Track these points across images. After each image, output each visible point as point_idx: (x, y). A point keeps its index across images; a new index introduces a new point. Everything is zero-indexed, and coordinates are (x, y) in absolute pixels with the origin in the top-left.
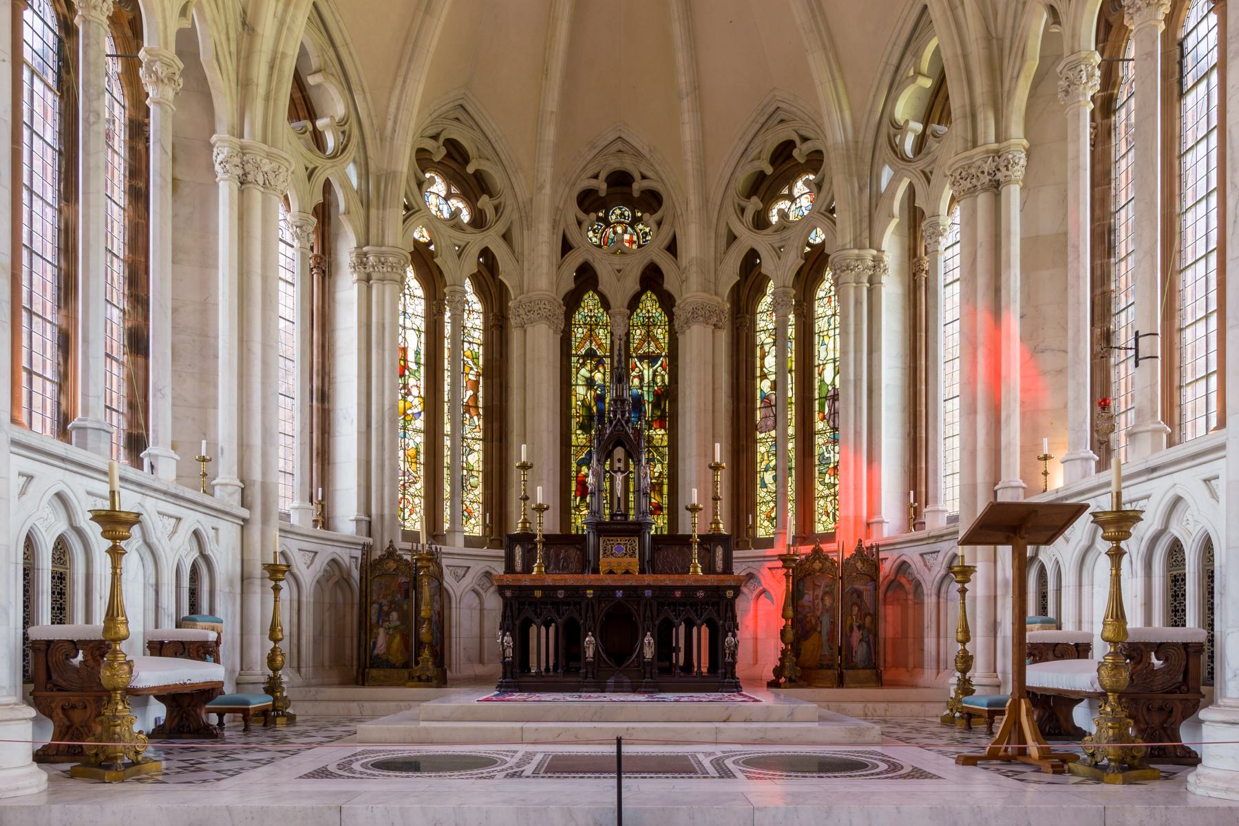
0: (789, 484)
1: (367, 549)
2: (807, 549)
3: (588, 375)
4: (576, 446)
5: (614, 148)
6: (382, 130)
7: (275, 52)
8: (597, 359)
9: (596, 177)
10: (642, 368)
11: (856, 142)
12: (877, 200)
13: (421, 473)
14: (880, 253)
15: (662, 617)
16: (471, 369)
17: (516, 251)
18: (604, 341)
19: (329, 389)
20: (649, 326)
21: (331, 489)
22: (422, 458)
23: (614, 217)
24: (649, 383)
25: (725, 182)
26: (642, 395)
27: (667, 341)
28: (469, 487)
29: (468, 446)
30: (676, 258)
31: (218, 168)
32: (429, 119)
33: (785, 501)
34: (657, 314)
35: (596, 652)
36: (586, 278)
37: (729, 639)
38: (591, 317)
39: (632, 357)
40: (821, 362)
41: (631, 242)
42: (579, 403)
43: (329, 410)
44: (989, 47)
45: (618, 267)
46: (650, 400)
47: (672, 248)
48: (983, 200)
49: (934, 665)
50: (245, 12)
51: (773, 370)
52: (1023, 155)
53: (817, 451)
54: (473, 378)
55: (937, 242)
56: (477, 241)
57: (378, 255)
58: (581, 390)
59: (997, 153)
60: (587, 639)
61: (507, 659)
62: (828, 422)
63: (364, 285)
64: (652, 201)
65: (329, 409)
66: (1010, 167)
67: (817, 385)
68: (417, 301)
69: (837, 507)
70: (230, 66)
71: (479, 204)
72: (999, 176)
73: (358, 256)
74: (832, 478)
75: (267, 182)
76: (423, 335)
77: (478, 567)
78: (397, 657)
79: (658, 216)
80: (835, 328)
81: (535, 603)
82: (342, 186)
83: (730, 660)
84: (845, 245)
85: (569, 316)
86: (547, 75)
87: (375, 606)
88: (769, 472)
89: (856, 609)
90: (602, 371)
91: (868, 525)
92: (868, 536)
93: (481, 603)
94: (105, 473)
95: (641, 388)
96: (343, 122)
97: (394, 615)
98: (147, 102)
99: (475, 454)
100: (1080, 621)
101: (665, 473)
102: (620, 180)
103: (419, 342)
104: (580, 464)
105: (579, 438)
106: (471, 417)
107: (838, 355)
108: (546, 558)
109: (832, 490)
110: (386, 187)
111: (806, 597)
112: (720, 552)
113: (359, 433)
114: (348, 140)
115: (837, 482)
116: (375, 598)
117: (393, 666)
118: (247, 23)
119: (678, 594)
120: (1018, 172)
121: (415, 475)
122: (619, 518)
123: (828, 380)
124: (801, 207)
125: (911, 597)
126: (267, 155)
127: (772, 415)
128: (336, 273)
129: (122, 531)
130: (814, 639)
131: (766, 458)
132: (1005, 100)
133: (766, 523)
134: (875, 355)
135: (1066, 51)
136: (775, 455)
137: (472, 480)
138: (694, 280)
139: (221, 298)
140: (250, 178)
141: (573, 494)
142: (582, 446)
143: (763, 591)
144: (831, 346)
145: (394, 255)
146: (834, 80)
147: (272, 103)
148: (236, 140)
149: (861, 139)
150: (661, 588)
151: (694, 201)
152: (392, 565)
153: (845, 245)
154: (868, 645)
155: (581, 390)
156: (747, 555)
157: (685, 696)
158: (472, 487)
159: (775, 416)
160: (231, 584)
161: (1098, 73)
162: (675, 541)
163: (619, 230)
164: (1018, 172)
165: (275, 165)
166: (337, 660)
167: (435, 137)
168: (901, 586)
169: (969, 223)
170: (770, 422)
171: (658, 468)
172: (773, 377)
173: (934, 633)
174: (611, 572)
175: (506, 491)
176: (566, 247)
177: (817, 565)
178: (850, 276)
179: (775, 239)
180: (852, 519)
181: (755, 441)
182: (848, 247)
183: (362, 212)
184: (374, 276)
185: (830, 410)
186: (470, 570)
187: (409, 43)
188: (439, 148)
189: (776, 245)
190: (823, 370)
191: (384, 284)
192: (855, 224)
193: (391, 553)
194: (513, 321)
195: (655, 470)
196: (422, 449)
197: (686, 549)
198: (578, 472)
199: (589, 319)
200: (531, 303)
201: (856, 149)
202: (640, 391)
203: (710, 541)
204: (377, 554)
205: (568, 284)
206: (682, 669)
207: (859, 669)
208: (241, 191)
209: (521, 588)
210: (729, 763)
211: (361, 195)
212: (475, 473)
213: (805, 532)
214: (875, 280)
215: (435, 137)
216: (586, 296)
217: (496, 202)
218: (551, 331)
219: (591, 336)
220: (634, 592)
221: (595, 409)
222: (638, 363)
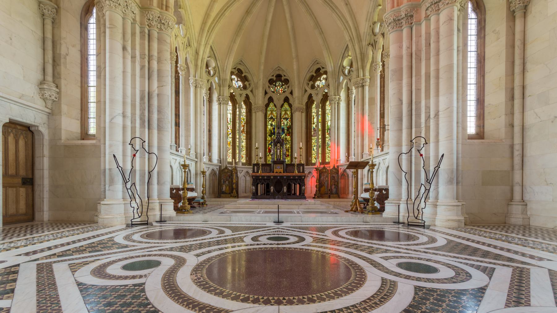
1: (220, 167)
2: (322, 166)
5: (278, 69)
6: (223, 69)
7: (202, 58)
9: (273, 76)
11: (334, 70)
13: (231, 148)
15: (288, 183)
22: (231, 144)
30: (292, 95)
31: (190, 84)
35: (273, 190)
36: (271, 100)
37: (303, 187)
41: (281, 90)
44: (361, 55)
47: (291, 93)
48: (360, 89)
49: (351, 193)
50: (196, 50)
53: (326, 142)
54: (243, 124)
55: (352, 96)
56: (244, 93)
57: (223, 98)
58: (269, 127)
59: (363, 79)
64: (287, 81)
67: (326, 126)
68: (230, 106)
70: (193, 62)
71: (245, 83)
72: (363, 84)
73: (218, 98)
77: (245, 170)
78: (228, 192)
79: (288, 85)
81: (259, 179)
82: (214, 83)
85: (266, 109)
89: (333, 180)
91: (337, 160)
92: (337, 163)
93: (246, 179)
94: (183, 157)
95: (284, 126)
96: (214, 68)
97: (227, 182)
100: (377, 184)
102: (279, 77)
103: (231, 116)
104: (269, 145)
105: (269, 138)
108: (262, 169)
111: (322, 178)
112: (301, 168)
116: (222, 178)
117: (227, 194)
120: (368, 83)
123: (329, 125)
125: (347, 178)
129: (186, 168)
130: (323, 187)
133: (314, 159)
134: (339, 121)
138: (297, 102)
140: (197, 86)
143: (313, 176)
145: (226, 98)
148: (194, 78)
150: (288, 176)
152: (226, 170)
154: (336, 189)
155: (269, 127)
157: (293, 200)
160: (194, 176)
161: (381, 66)
162: (292, 165)
163: (279, 87)
164: (368, 83)
166: (213, 192)
167: (235, 69)
168: (344, 175)
169: (357, 93)
173: (351, 186)
174: (277, 172)
176: (266, 93)
177: (324, 170)
178: (333, 102)
179: (316, 92)
180: (333, 160)
181: (312, 139)
183: (219, 88)
184: (222, 103)
187: (230, 49)
193: (226, 168)
194: (253, 111)
197: (294, 167)
198: (269, 147)
201: (334, 72)
203: (300, 165)
204: (222, 168)
205: (266, 102)
206: (293, 194)
208: (195, 89)
209: (257, 176)
210: (300, 212)
213: (324, 162)
215: (235, 69)
219: (272, 113)
220: (282, 177)
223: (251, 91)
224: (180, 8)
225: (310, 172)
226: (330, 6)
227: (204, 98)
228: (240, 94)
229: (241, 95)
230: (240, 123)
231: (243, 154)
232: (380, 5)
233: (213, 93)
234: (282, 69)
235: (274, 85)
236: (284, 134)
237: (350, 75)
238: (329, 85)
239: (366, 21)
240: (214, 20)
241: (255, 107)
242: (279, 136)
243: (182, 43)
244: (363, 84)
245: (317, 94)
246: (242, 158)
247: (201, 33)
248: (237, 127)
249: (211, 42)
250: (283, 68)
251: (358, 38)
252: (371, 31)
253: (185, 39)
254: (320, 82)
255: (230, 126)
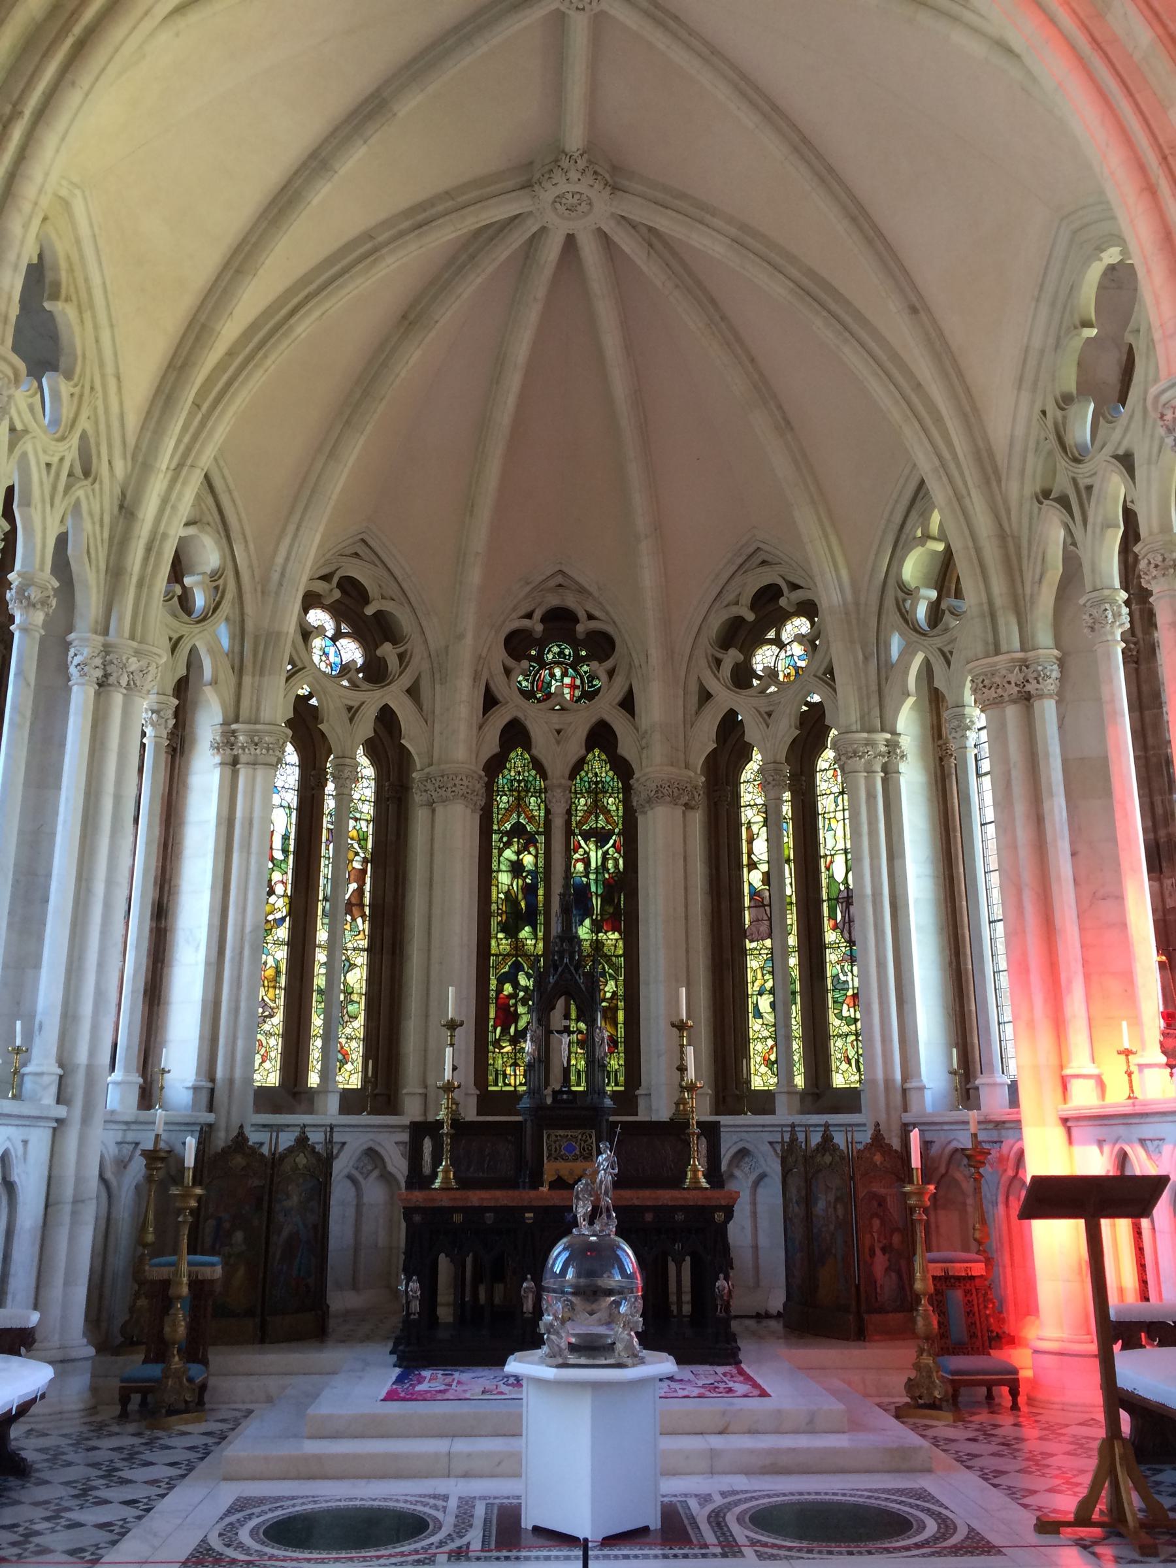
0: (794, 1015)
3: (514, 858)
4: (497, 955)
5: (552, 583)
6: (265, 580)
8: (526, 837)
9: (529, 616)
10: (587, 849)
12: (886, 672)
13: (281, 1002)
14: (895, 737)
16: (357, 854)
17: (424, 707)
18: (536, 813)
19: (168, 901)
20: (597, 794)
21: (158, 1040)
23: (550, 656)
24: (597, 868)
25: (695, 629)
26: (588, 885)
27: (621, 814)
28: (346, 1018)
29: (348, 959)
30: (633, 717)
31: (73, 670)
32: (322, 561)
33: (789, 1038)
34: (608, 779)
37: (721, 1283)
38: (519, 782)
39: (574, 834)
40: (828, 853)
41: (573, 687)
42: (502, 896)
43: (165, 930)
45: (557, 727)
46: (600, 892)
47: (628, 704)
51: (765, 857)
52: (1055, 667)
53: (830, 971)
54: (357, 865)
55: (964, 737)
56: (373, 700)
57: (251, 735)
58: (504, 878)
59: (1024, 664)
60: (525, 1285)
61: (412, 1317)
62: (842, 932)
63: (228, 770)
65: (165, 927)
66: (1040, 679)
67: (824, 883)
69: (861, 1051)
71: (379, 652)
73: (223, 734)
74: (852, 1010)
75: (132, 683)
76: (294, 814)
79: (609, 664)
80: (844, 810)
82: (211, 651)
83: (723, 1314)
84: (851, 725)
85: (490, 791)
86: (472, 511)
87: (211, 1223)
88: (765, 997)
90: (533, 852)
93: (359, 1195)
95: (587, 876)
96: (216, 575)
97: (239, 1236)
98: (12, 628)
99: (357, 970)
101: (620, 992)
104: (501, 981)
105: (500, 943)
106: (354, 919)
107: (848, 846)
109: (853, 1027)
110: (266, 648)
113: (207, 964)
114: (222, 597)
115: (858, 1016)
118: (126, 505)
119: (649, 1217)
121: (272, 1005)
122: (565, 1096)
123: (839, 875)
124: (792, 655)
126: (135, 652)
127: (765, 918)
128: (190, 751)
131: (759, 976)
132: (1028, 608)
133: (763, 1069)
134: (897, 863)
135: (1088, 588)
136: (772, 973)
137: (350, 1008)
139: (60, 828)
140: (111, 680)
141: (491, 1023)
142: (505, 955)
144: (840, 833)
145: (270, 733)
146: (826, 537)
147: (145, 590)
148: (100, 639)
149: (862, 600)
151: (656, 655)
152: (239, 1160)
153: (851, 725)
154: (900, 1278)
155: (504, 878)
156: (737, 1123)
158: (350, 1017)
159: (770, 919)
163: (558, 672)
164: (1050, 686)
165: (143, 663)
167: (326, 578)
170: (764, 928)
171: (610, 987)
172: (764, 867)
175: (399, 1024)
176: (490, 701)
181: (744, 953)
182: (854, 728)
183: (233, 680)
184: (243, 758)
185: (843, 917)
186: (346, 1146)
188: (331, 590)
189: (763, 710)
190: (832, 862)
191: (255, 769)
192: (861, 700)
194: (418, 797)
195: (606, 989)
196: (283, 968)
199: (516, 784)
200: (443, 776)
202: (585, 880)
205: (492, 746)
207: (888, 1312)
208: (98, 694)
211: (233, 659)
212: (355, 997)
214: (891, 768)
216: (513, 755)
217: (401, 650)
218: (469, 811)
219: (519, 805)
221: (523, 904)
222: (582, 843)
223: (409, 691)
224: (55, 296)
225: (743, 1153)
226: (829, 312)
227: (144, 734)
228: (350, 708)
229: (352, 712)
230: (340, 862)
231: (349, 1038)
232: (1087, 324)
233: (195, 704)
234: (577, 583)
235: (531, 658)
236: (587, 922)
237: (946, 630)
238: (830, 671)
239: (1019, 388)
240: (231, 354)
241: (428, 778)
242: (572, 958)
243: (48, 465)
244: (1028, 687)
245: (769, 714)
246: (344, 1062)
247: (156, 414)
248: (322, 881)
249: (206, 458)
250: (581, 580)
251: (979, 460)
252: (1052, 437)
253: (62, 447)
254: (775, 649)
255: (283, 880)
